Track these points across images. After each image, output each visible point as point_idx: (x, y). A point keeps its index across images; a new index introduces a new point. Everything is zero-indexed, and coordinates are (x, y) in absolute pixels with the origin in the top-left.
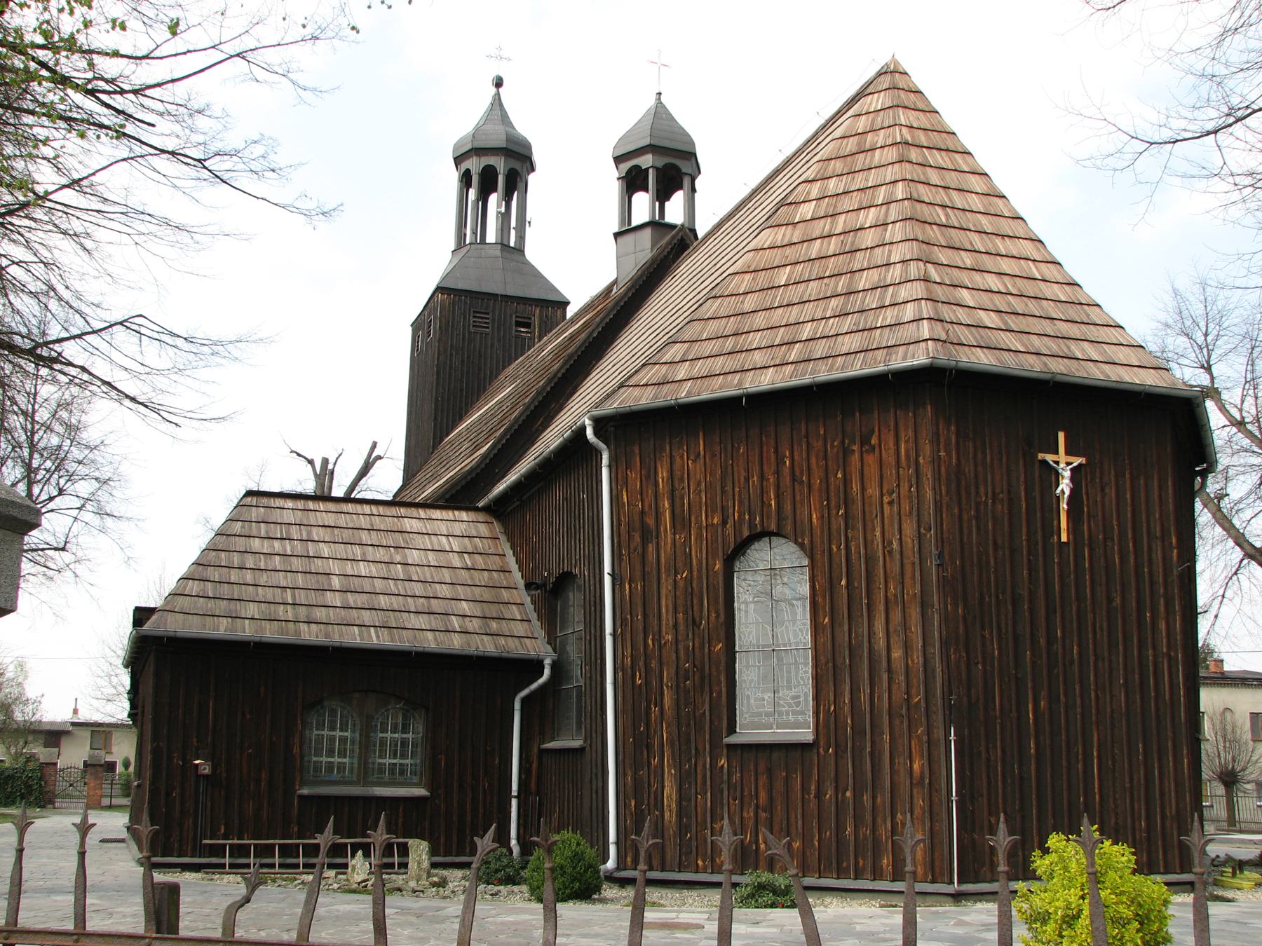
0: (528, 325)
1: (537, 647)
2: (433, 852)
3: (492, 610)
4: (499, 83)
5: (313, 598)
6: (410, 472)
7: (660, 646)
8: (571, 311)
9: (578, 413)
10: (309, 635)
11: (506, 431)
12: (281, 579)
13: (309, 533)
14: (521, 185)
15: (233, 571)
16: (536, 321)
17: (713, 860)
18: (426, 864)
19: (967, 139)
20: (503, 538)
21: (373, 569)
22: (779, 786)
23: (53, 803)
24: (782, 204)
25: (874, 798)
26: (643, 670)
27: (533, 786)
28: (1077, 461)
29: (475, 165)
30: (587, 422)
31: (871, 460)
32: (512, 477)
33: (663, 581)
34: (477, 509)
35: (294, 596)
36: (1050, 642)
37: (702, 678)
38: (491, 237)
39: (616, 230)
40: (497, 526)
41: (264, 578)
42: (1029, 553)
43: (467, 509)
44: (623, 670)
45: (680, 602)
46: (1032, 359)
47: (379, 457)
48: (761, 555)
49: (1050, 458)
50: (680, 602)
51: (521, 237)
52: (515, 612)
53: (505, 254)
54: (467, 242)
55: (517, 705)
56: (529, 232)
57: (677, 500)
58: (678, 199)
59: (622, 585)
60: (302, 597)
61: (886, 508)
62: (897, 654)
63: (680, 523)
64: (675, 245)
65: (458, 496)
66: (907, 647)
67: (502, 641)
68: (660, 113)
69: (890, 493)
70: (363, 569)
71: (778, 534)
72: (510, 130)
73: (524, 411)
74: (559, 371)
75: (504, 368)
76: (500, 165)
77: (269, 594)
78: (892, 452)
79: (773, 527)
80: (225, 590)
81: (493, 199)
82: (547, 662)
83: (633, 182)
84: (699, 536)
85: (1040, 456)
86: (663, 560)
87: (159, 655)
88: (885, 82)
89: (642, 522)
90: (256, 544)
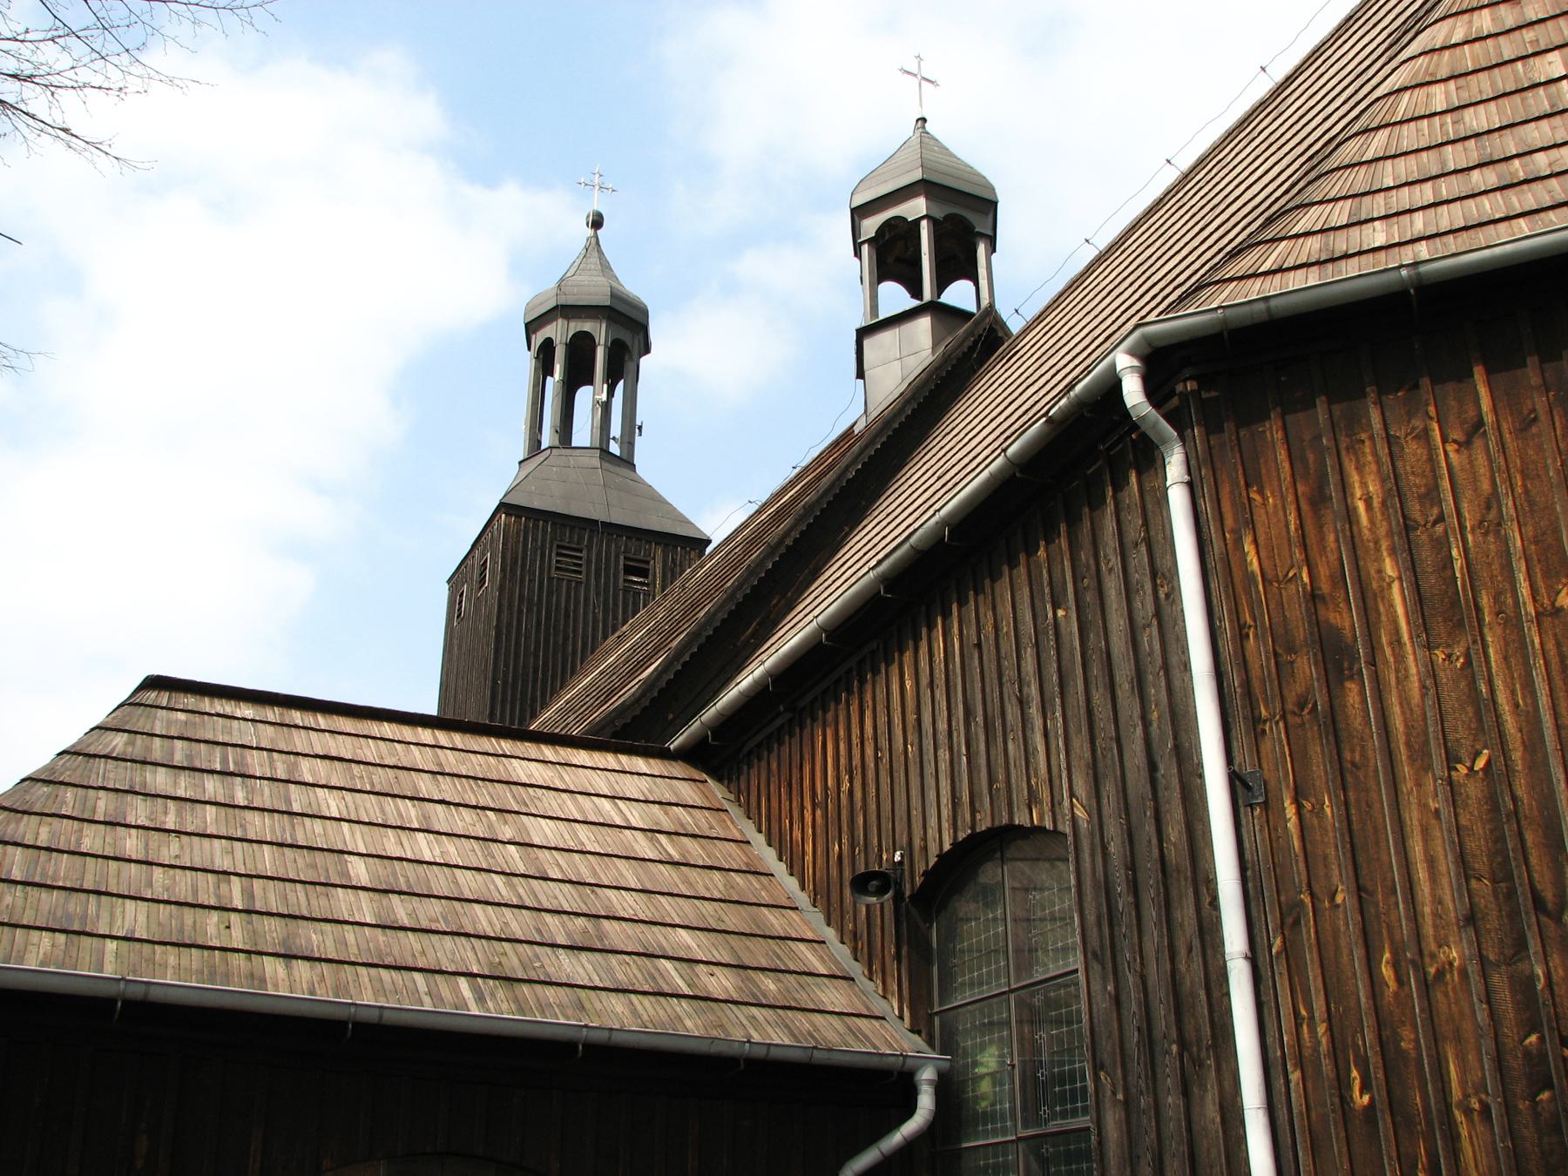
0: (643, 573)
1: (889, 1036)
3: (753, 950)
4: (597, 222)
5: (299, 899)
7: (1426, 987)
10: (289, 984)
11: (693, 637)
12: (219, 855)
13: (293, 768)
15: (89, 830)
16: (657, 567)
20: (735, 811)
21: (452, 850)
26: (1374, 1059)
29: (559, 332)
30: (1123, 361)
32: (746, 680)
33: (1408, 785)
34: (665, 755)
35: (249, 894)
38: (583, 434)
39: (861, 322)
40: (717, 791)
41: (170, 850)
43: (645, 753)
44: (1300, 1064)
51: (628, 442)
52: (810, 958)
53: (606, 465)
54: (548, 439)
56: (640, 442)
57: (1426, 556)
59: (1269, 806)
60: (269, 896)
63: (1441, 611)
64: (976, 345)
67: (802, 1021)
70: (425, 847)
72: (614, 284)
73: (725, 601)
74: (787, 533)
75: (605, 638)
76: (600, 332)
77: (183, 885)
80: (62, 869)
82: (927, 1075)
84: (1517, 648)
86: (1398, 723)
89: (1316, 623)
90: (160, 780)
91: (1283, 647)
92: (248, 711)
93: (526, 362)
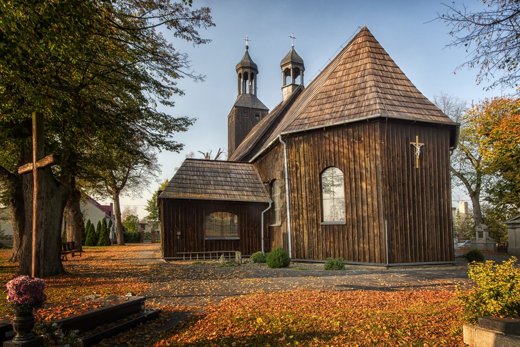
0: (258, 116)
2: (242, 254)
6: (230, 156)
8: (269, 112)
9: (277, 134)
14: (254, 77)
16: (260, 115)
17: (318, 256)
18: (240, 258)
19: (387, 50)
22: (336, 236)
23: (142, 241)
24: (333, 72)
25: (363, 239)
27: (267, 236)
28: (422, 144)
31: (361, 145)
34: (249, 163)
36: (413, 196)
37: (314, 207)
38: (248, 92)
42: (407, 171)
43: (246, 163)
45: (307, 186)
46: (409, 114)
47: (221, 152)
48: (327, 174)
49: (414, 144)
50: (307, 186)
51: (255, 92)
55: (262, 215)
58: (299, 78)
61: (366, 159)
62: (369, 200)
65: (244, 159)
66: (372, 197)
68: (293, 52)
69: (367, 154)
71: (334, 167)
76: (248, 71)
78: (368, 142)
79: (333, 165)
81: (248, 81)
83: (287, 73)
85: (411, 143)
87: (167, 205)
88: (363, 34)
91: (293, 165)
92: (198, 162)
93: (236, 75)
